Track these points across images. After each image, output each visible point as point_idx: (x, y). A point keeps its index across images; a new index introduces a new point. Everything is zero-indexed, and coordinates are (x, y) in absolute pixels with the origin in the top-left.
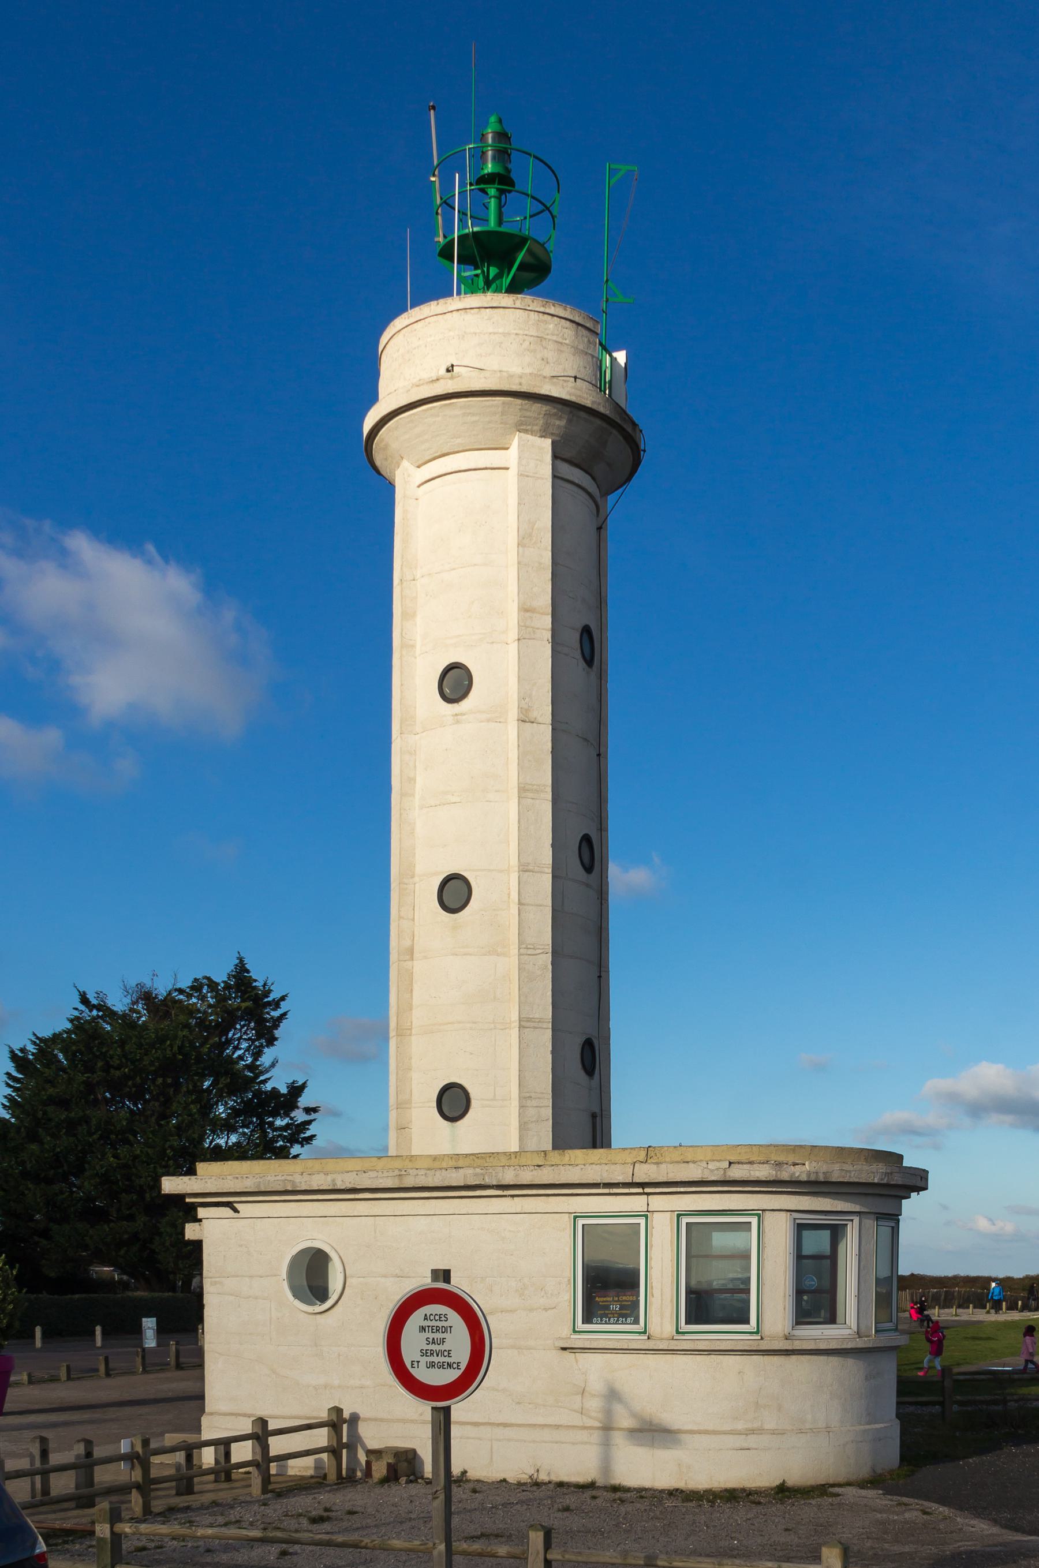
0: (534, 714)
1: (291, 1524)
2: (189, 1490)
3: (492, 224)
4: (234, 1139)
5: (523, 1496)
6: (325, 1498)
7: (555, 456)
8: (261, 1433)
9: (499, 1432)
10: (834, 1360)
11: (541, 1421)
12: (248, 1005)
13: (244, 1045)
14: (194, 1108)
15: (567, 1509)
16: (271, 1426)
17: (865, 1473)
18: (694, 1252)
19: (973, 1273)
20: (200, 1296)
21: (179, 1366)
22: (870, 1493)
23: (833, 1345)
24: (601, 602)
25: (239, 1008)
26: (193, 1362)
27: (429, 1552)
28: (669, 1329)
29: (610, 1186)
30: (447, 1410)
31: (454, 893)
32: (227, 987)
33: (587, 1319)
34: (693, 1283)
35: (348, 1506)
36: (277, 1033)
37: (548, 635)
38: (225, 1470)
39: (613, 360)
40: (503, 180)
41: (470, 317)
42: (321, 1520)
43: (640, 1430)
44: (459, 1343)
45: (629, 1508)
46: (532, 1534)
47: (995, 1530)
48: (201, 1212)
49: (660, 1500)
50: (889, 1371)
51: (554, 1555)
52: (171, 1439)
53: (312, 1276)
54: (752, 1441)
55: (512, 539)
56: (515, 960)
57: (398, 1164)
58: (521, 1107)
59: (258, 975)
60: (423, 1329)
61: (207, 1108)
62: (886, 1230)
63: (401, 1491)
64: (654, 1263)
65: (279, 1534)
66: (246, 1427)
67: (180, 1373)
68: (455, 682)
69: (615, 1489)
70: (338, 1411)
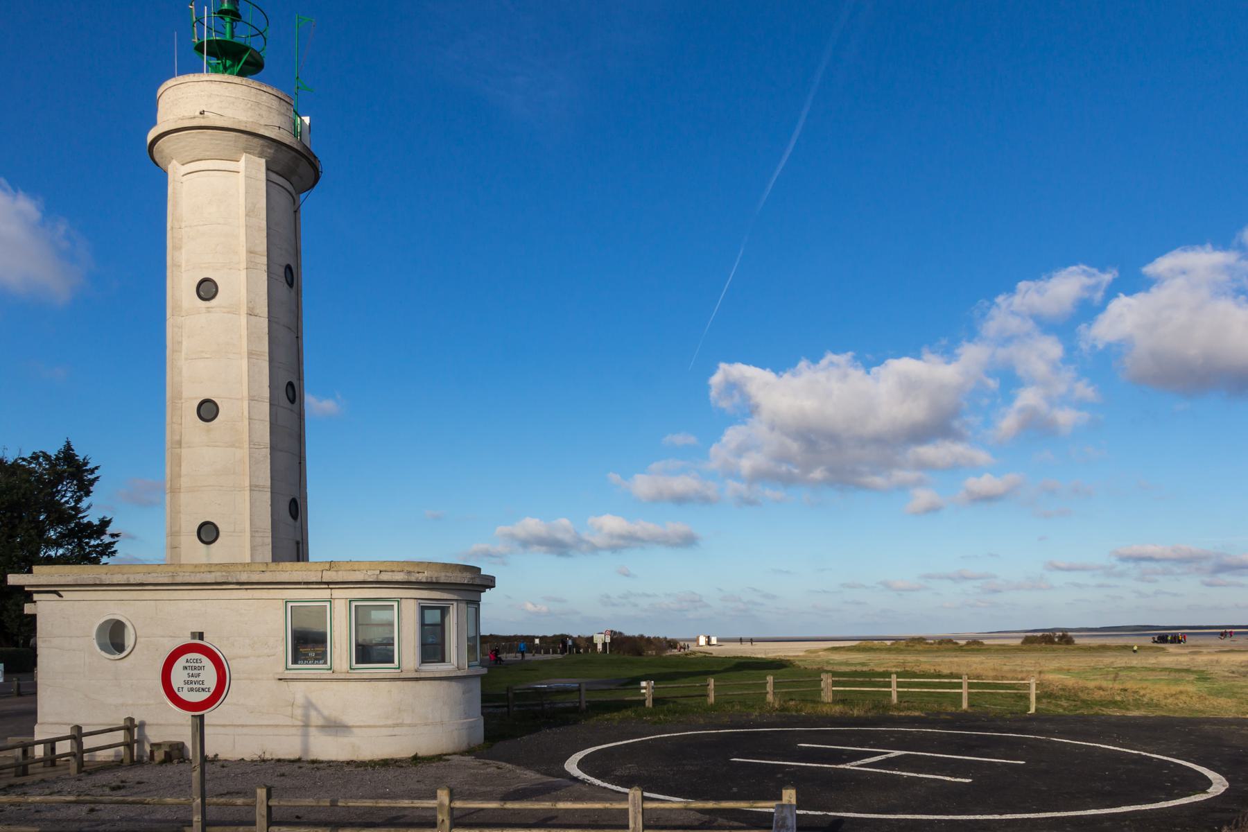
0: (257, 311)
1: (99, 791)
2: (25, 773)
3: (228, 37)
4: (61, 551)
5: (254, 768)
6: (121, 774)
7: (268, 169)
8: (77, 735)
9: (239, 730)
10: (445, 683)
11: (266, 723)
12: (73, 470)
13: (69, 495)
14: (33, 532)
15: (283, 775)
16: (84, 730)
17: (464, 747)
18: (360, 621)
19: (525, 634)
20: (35, 649)
21: (19, 694)
22: (467, 758)
23: (443, 675)
24: (297, 253)
25: (64, 471)
26: (30, 692)
27: (190, 805)
28: (346, 666)
29: (308, 584)
30: (202, 717)
31: (207, 410)
32: (57, 458)
33: (295, 661)
34: (360, 641)
35: (137, 779)
36: (92, 489)
37: (265, 268)
38: (51, 759)
39: (302, 121)
40: (235, 15)
41: (214, 86)
42: (119, 788)
43: (323, 727)
44: (209, 676)
45: (322, 772)
46: (259, 791)
47: (538, 776)
48: (36, 597)
49: (342, 768)
50: (477, 686)
51: (273, 803)
52: (12, 740)
53: (114, 637)
54: (397, 731)
55: (242, 211)
56: (246, 451)
57: (171, 569)
58: (252, 536)
59: (80, 453)
60: (185, 668)
61: (42, 532)
62: (472, 610)
63: (173, 769)
64: (335, 628)
65: (88, 798)
66: (67, 731)
67: (20, 698)
68: (207, 289)
69: (313, 762)
70: (131, 720)
